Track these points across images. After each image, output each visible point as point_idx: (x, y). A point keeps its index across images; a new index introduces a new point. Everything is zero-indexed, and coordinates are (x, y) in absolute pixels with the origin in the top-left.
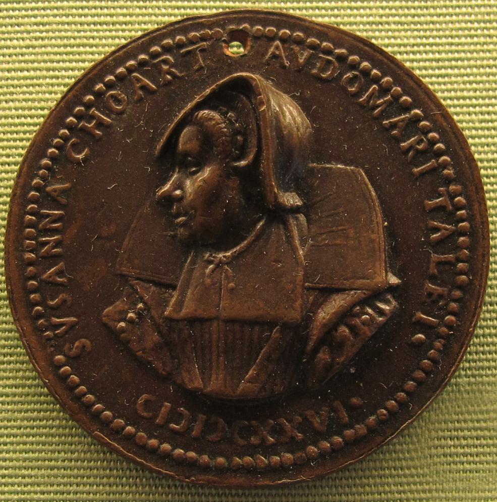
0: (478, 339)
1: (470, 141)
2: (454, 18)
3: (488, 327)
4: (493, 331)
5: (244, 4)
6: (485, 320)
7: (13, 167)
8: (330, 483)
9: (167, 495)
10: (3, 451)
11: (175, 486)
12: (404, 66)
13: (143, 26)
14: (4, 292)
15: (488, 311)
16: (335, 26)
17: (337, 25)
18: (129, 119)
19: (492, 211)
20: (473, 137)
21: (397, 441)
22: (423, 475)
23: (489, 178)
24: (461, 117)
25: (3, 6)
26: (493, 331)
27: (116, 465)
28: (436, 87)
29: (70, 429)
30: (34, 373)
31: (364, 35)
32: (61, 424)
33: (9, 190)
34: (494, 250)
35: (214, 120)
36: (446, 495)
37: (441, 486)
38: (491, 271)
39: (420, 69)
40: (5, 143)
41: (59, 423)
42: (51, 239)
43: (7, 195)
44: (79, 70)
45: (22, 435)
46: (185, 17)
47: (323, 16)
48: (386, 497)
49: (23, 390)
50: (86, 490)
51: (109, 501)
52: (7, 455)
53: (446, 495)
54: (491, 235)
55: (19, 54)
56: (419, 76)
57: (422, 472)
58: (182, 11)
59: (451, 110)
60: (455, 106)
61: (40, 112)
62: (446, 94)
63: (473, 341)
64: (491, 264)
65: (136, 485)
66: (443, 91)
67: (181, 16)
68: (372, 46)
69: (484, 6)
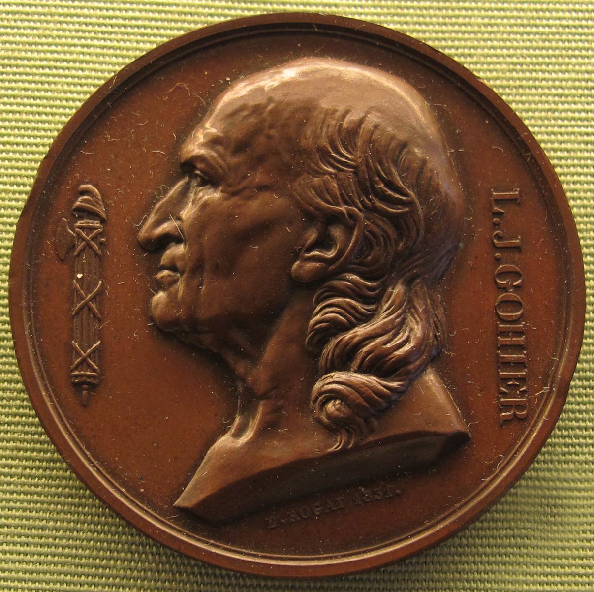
1: (568, 195)
7: (33, 165)
9: (199, 585)
11: (201, 574)
12: (439, 130)
19: (588, 275)
21: (463, 534)
23: (589, 381)
24: (549, 145)
26: (591, 536)
27: (178, 585)
28: (501, 90)
29: (162, 582)
30: (56, 455)
32: (94, 503)
34: (588, 258)
35: (77, 302)
36: (503, 508)
37: (452, 576)
39: (517, 103)
40: (6, 61)
41: (96, 511)
42: (93, 188)
43: (9, 240)
44: (65, 115)
45: (16, 527)
47: (450, 48)
48: (441, 569)
49: (10, 411)
50: (21, 438)
51: (512, 591)
56: (516, 110)
59: (562, 178)
60: (555, 150)
63: (573, 391)
65: (159, 572)
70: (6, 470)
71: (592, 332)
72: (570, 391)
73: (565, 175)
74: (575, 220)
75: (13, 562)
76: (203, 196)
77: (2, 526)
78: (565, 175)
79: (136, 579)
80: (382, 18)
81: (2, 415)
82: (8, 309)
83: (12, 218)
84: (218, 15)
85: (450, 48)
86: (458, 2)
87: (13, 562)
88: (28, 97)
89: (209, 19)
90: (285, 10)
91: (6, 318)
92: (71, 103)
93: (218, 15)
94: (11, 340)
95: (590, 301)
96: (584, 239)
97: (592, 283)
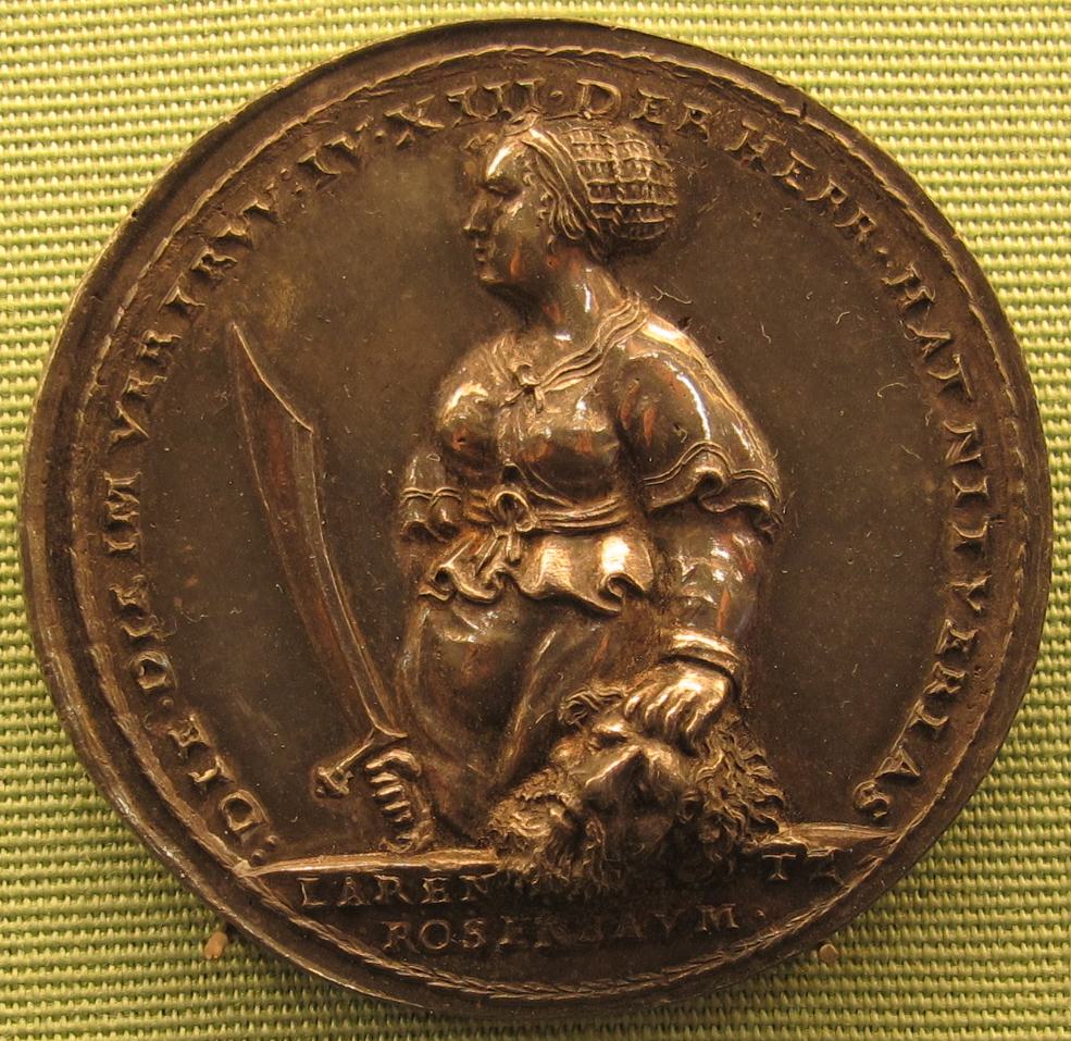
0: (1043, 695)
2: (43, 250)
3: (1051, 739)
4: (1064, 748)
5: (450, 9)
6: (1035, 704)
8: (738, 1016)
10: (9, 359)
13: (303, 51)
14: (11, 784)
15: (1035, 704)
16: (730, 56)
17: (733, 54)
18: (277, 281)
20: (1017, 305)
22: (963, 892)
25: (3, 6)
26: (1064, 748)
28: (943, 193)
31: (793, 79)
33: (15, 464)
36: (975, 816)
38: (1057, 488)
44: (162, 153)
46: (429, 24)
51: (247, 1039)
52: (139, 1021)
53: (975, 816)
54: (1055, 512)
55: (50, 109)
57: (932, 885)
58: (362, 30)
61: (38, 332)
62: (966, 210)
64: (1057, 507)
66: (958, 203)
67: (420, 20)
68: (809, 106)
69: (265, 12)
70: (12, 151)
71: (1062, 660)
72: (1034, 679)
73: (1002, 271)
74: (1028, 362)
75: (27, 984)
76: (386, 784)
77: (4, 113)
78: (1002, 271)
79: (249, 1007)
80: (737, 43)
81: (4, 699)
82: (24, 616)
83: (19, 632)
84: (393, 21)
85: (716, 36)
86: (769, 6)
87: (27, 984)
88: (51, 879)
89: (362, 30)
90: (460, 17)
91: (10, 517)
92: (38, 332)
93: (393, 21)
94: (67, 744)
95: (1058, 482)
96: (1049, 402)
97: (1065, 544)
